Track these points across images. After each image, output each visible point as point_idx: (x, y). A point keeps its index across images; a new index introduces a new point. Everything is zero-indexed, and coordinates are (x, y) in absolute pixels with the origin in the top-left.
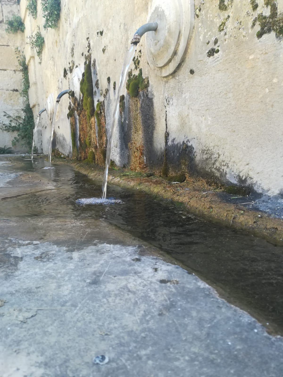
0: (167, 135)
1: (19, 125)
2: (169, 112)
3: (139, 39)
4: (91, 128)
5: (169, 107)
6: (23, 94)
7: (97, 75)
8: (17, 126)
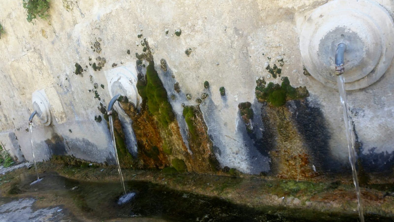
7: (174, 77)
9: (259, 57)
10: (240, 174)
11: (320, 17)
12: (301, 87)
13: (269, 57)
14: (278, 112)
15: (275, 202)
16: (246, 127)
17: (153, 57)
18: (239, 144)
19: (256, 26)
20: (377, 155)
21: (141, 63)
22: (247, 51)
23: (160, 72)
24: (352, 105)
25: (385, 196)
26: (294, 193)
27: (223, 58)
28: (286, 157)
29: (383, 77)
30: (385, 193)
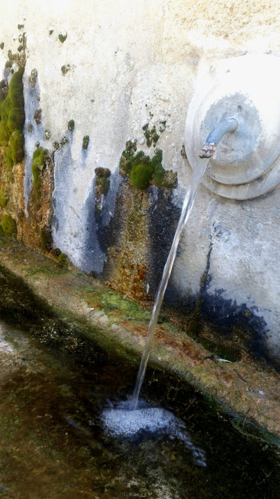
7: (39, 100)
9: (141, 109)
10: (69, 264)
11: (226, 72)
12: (171, 171)
13: (152, 113)
14: (136, 196)
15: (81, 310)
16: (95, 203)
17: (26, 63)
18: (81, 223)
19: (152, 60)
20: (222, 301)
21: (11, 66)
22: (131, 93)
23: (26, 86)
24: (219, 220)
25: (206, 358)
26: (109, 309)
27: (102, 94)
28: (124, 262)
29: (270, 193)
30: (210, 354)
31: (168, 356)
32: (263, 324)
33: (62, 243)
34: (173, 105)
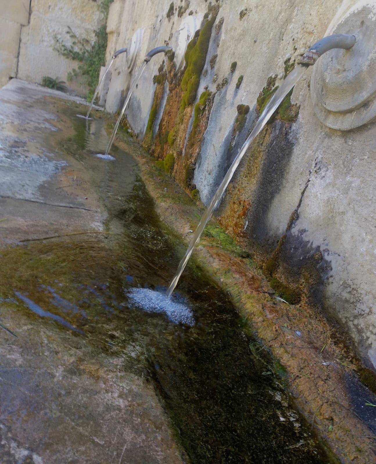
0: (295, 217)
1: (84, 53)
2: (313, 185)
3: (315, 60)
4: (182, 120)
5: (316, 177)
6: (102, 8)
7: (218, 46)
8: (81, 53)
31: (230, 280)
32: (329, 269)
33: (199, 179)
34: (315, 37)
